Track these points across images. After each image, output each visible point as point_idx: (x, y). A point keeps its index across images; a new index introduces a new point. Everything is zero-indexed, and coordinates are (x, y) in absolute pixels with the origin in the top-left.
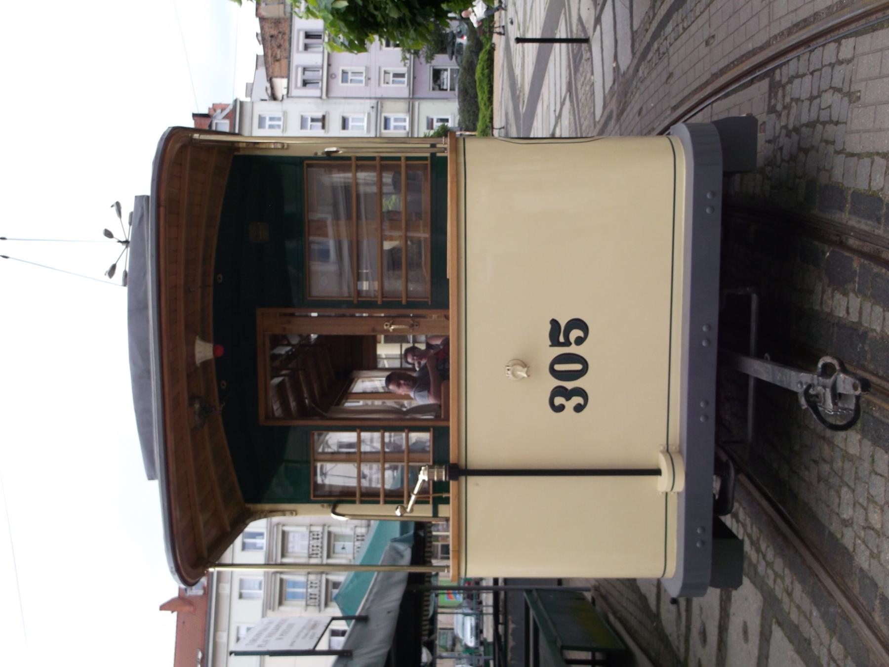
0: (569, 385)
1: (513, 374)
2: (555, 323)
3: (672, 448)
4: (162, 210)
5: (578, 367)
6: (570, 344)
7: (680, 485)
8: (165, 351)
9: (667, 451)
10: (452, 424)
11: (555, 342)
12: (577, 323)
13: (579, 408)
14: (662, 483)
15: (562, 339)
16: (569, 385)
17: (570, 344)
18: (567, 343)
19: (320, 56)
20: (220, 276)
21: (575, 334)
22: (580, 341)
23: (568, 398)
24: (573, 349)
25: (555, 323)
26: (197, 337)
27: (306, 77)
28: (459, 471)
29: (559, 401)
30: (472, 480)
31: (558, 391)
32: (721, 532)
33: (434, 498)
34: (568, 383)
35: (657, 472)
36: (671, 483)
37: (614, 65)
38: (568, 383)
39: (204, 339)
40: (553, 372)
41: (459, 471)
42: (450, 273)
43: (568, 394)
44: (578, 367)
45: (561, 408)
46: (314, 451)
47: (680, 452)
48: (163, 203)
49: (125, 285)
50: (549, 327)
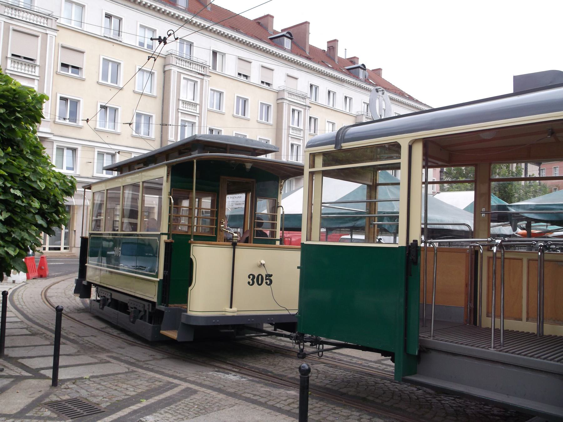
0: (255, 280)
2: (271, 276)
5: (260, 283)
11: (266, 276)
12: (271, 281)
13: (249, 283)
14: (228, 309)
16: (255, 280)
19: (545, 258)
21: (268, 281)
22: (266, 283)
24: (265, 281)
25: (271, 276)
27: (295, 111)
28: (234, 245)
29: (251, 277)
31: (254, 276)
33: (214, 211)
34: (256, 280)
35: (231, 307)
36: (230, 312)
38: (256, 280)
41: (234, 245)
43: (253, 280)
44: (260, 283)
45: (249, 277)
46: (530, 162)
49: (19, 272)
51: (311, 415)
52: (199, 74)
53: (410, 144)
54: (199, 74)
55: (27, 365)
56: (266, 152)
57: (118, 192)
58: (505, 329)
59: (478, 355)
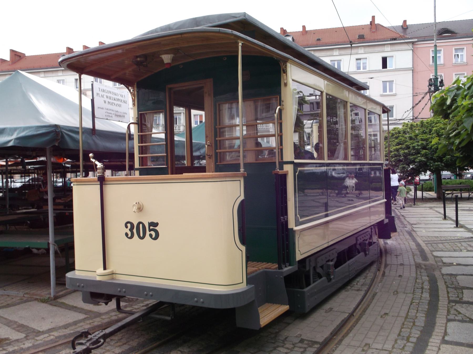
0: (135, 231)
1: (134, 205)
2: (156, 225)
3: (114, 276)
4: (180, 36)
5: (141, 235)
6: (150, 231)
7: (98, 278)
8: (214, 34)
9: (113, 274)
10: (170, 176)
13: (127, 234)
14: (100, 270)
15: (151, 227)
16: (135, 231)
17: (150, 231)
18: (150, 230)
20: (226, 59)
21: (153, 233)
22: (151, 235)
23: (130, 230)
24: (148, 233)
25: (156, 225)
26: (172, 55)
29: (129, 225)
30: (99, 186)
32: (107, 298)
35: (105, 268)
37: (455, 264)
38: (144, 230)
39: (173, 60)
40: (140, 223)
42: (185, 175)
43: (131, 230)
44: (141, 235)
45: (127, 227)
47: (113, 279)
48: (183, 36)
50: (156, 222)
51: (471, 300)
52: (327, 252)
53: (411, 203)
54: (327, 252)
55: (246, 303)
56: (375, 151)
57: (77, 163)
58: (309, 110)
59: (193, 177)
